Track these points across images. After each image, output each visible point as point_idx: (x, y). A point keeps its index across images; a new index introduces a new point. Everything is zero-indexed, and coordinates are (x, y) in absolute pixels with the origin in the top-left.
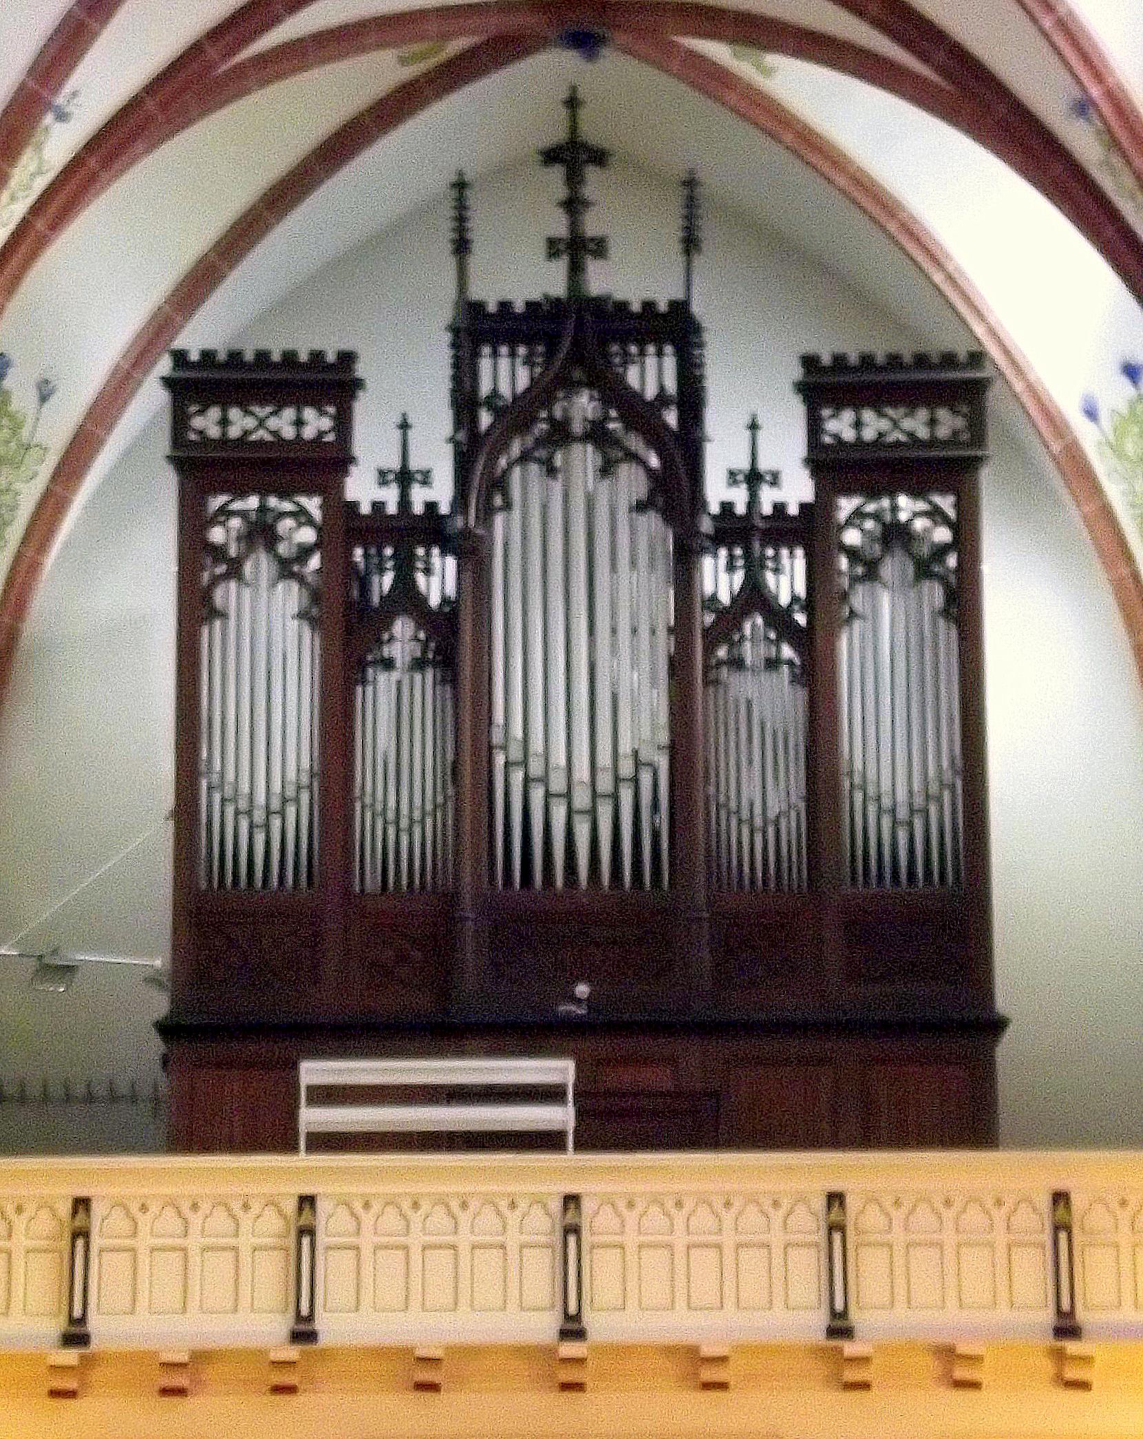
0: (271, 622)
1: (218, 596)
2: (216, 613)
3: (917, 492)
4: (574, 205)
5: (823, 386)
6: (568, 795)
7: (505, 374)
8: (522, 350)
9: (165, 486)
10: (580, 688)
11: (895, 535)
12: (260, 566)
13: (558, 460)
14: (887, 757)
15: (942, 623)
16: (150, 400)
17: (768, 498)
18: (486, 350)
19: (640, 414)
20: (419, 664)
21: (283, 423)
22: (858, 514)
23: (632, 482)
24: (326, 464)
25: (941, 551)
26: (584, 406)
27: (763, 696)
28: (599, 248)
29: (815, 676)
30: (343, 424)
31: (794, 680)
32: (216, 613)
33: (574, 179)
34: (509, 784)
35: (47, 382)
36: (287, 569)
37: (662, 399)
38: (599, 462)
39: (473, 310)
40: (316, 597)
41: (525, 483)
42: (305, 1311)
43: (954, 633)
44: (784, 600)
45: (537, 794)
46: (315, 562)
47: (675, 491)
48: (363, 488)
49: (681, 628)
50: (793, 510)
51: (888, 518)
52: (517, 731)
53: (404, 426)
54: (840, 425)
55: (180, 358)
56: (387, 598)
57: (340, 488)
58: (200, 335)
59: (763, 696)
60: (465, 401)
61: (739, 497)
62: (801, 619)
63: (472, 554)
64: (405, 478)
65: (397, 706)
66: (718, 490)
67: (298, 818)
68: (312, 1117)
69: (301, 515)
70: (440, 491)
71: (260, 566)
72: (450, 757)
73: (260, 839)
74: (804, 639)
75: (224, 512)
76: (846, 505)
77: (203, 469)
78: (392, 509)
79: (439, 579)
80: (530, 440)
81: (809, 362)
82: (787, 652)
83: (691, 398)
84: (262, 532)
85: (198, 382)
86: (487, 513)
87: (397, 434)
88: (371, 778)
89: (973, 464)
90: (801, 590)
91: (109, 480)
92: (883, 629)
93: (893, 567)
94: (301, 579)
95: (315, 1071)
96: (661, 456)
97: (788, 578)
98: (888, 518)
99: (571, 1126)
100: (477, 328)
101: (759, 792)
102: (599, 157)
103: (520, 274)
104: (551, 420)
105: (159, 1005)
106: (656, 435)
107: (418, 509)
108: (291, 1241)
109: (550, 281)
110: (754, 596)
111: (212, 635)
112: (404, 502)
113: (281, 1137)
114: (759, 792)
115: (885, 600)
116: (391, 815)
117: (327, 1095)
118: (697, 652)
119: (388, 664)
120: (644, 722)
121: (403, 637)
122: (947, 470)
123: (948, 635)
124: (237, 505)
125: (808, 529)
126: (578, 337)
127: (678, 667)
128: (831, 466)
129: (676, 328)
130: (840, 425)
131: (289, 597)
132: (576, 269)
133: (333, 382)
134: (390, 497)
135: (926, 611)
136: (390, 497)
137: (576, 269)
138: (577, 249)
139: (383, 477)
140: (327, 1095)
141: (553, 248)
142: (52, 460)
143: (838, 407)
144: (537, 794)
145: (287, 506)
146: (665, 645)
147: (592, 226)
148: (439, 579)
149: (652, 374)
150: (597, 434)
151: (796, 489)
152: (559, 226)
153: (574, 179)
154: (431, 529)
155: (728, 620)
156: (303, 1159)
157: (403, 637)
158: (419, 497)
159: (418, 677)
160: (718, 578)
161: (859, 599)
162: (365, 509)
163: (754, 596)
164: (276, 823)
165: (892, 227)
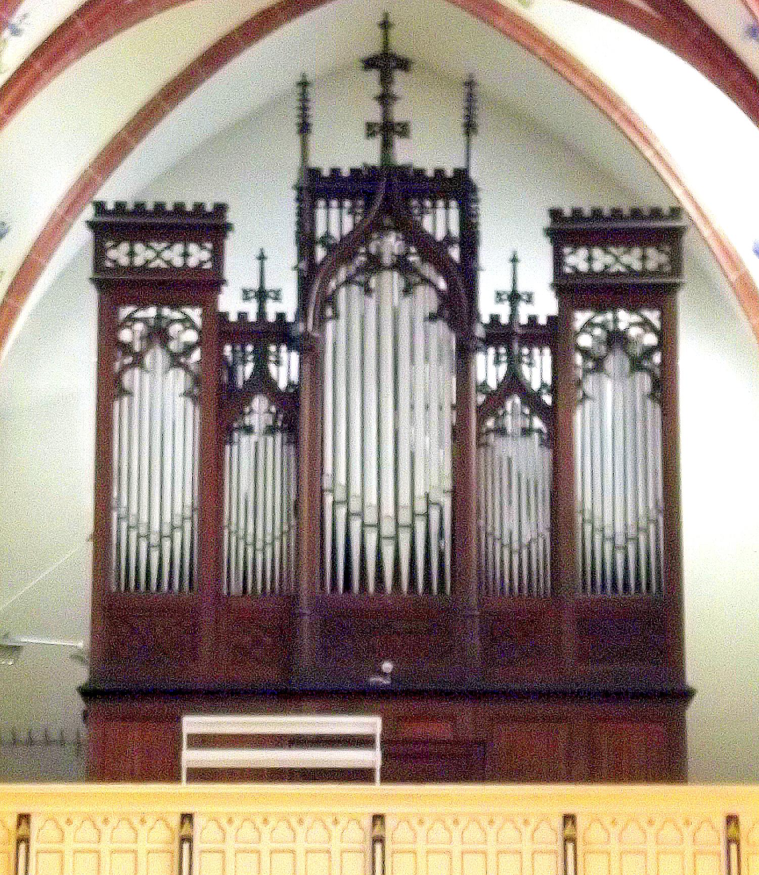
0: (164, 400)
2: (123, 392)
3: (632, 308)
4: (385, 99)
5: (566, 231)
6: (378, 526)
7: (334, 220)
8: (347, 204)
9: (89, 300)
10: (388, 448)
11: (616, 339)
12: (156, 358)
13: (373, 283)
14: (610, 501)
16: (78, 238)
17: (524, 312)
19: (432, 250)
20: (271, 430)
21: (174, 255)
22: (590, 324)
23: (426, 300)
24: (204, 285)
25: (649, 352)
27: (519, 455)
28: (404, 130)
29: (557, 441)
30: (218, 256)
31: (543, 443)
32: (123, 392)
33: (386, 80)
34: (335, 517)
36: (176, 360)
37: (449, 240)
39: (313, 174)
40: (197, 381)
43: (658, 410)
47: (457, 306)
48: (231, 303)
49: (461, 405)
51: (611, 327)
55: (100, 207)
56: (251, 381)
57: (215, 302)
58: (117, 190)
59: (519, 455)
60: (306, 241)
62: (548, 399)
63: (310, 351)
64: (262, 295)
65: (255, 457)
66: (489, 306)
67: (183, 541)
68: (191, 757)
69: (187, 322)
70: (287, 305)
71: (156, 358)
72: (293, 497)
74: (550, 414)
75: (131, 319)
76: (581, 318)
77: (116, 288)
79: (286, 368)
80: (352, 269)
81: (555, 214)
82: (538, 423)
83: (469, 239)
84: (158, 334)
85: (113, 225)
86: (321, 321)
87: (257, 263)
88: (236, 513)
89: (671, 289)
92: (607, 408)
93: (615, 362)
94: (186, 368)
95: (193, 724)
96: (447, 281)
97: (538, 369)
98: (611, 327)
100: (316, 188)
101: (516, 526)
102: (404, 65)
103: (346, 148)
104: (368, 254)
105: (81, 675)
106: (443, 266)
107: (271, 318)
109: (367, 154)
110: (513, 383)
111: (120, 407)
113: (169, 771)
114: (516, 526)
117: (202, 741)
118: (472, 423)
120: (434, 474)
121: (259, 411)
122: (654, 293)
123: (654, 412)
124: (141, 314)
125: (553, 335)
126: (388, 194)
127: (459, 433)
128: (572, 290)
129: (458, 188)
130: (577, 260)
131: (178, 381)
132: (387, 145)
133: (210, 226)
137: (387, 145)
138: (388, 130)
140: (202, 741)
141: (371, 130)
143: (576, 246)
145: (177, 315)
146: (449, 418)
147: (399, 114)
148: (286, 368)
149: (441, 221)
150: (401, 265)
151: (545, 306)
152: (375, 114)
153: (386, 80)
154: (281, 332)
155: (495, 401)
157: (259, 411)
158: (272, 310)
159: (270, 439)
160: (488, 369)
161: (589, 385)
162: (233, 318)
163: (513, 383)
164: (167, 544)
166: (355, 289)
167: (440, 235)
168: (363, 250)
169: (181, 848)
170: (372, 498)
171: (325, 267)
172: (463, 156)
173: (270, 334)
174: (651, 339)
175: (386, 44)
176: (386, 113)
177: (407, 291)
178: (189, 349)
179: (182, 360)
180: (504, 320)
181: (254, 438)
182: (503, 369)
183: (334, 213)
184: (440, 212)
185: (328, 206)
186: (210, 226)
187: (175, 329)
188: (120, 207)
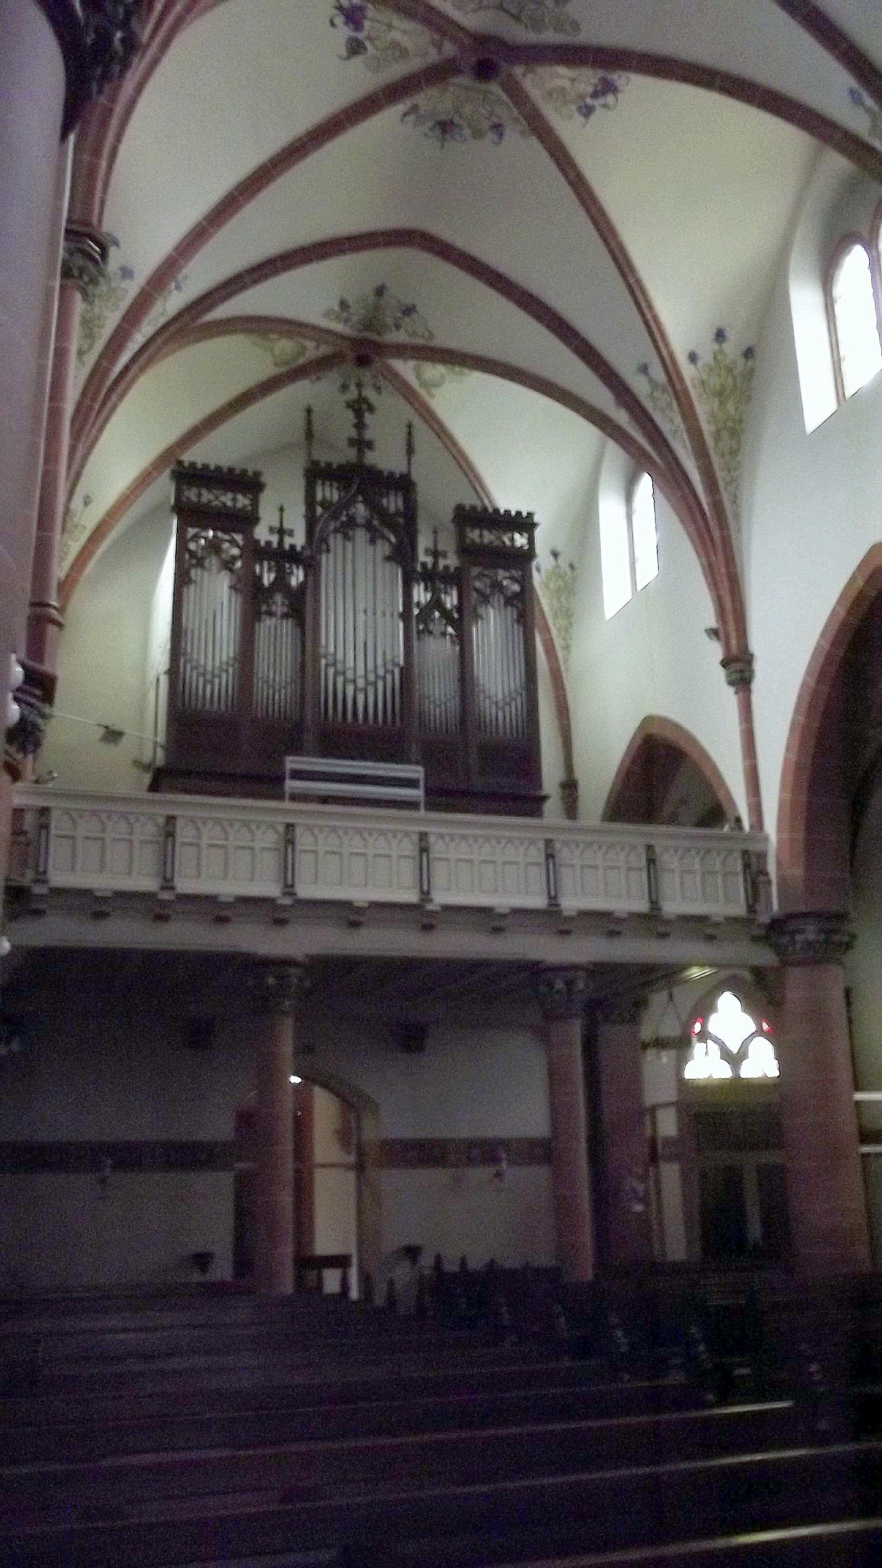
0: (218, 591)
7: (327, 492)
12: (213, 562)
13: (351, 533)
18: (320, 482)
20: (285, 616)
21: (227, 499)
23: (382, 548)
26: (361, 510)
27: (438, 650)
29: (463, 640)
30: (255, 504)
31: (453, 642)
35: (88, 497)
36: (227, 565)
40: (239, 580)
43: (521, 629)
45: (340, 680)
46: (239, 564)
53: (282, 509)
54: (192, 494)
55: (180, 463)
57: (251, 532)
58: (200, 454)
60: (310, 502)
61: (429, 560)
62: (456, 615)
63: (312, 567)
64: (281, 532)
65: (276, 632)
66: (423, 557)
68: (291, 785)
69: (233, 542)
70: (298, 539)
71: (213, 562)
72: (299, 659)
75: (196, 537)
76: (475, 571)
78: (275, 545)
80: (338, 524)
82: (450, 630)
87: (277, 514)
91: (115, 543)
94: (231, 570)
95: (292, 763)
96: (396, 537)
97: (450, 600)
98: (494, 578)
99: (422, 799)
100: (315, 474)
104: (347, 515)
106: (393, 527)
107: (287, 546)
109: (351, 455)
111: (190, 592)
113: (280, 797)
117: (298, 775)
121: (279, 603)
123: (518, 630)
124: (203, 534)
128: (466, 551)
132: (361, 453)
133: (249, 483)
134: (275, 539)
136: (275, 539)
137: (361, 453)
139: (271, 530)
140: (298, 775)
142: (87, 534)
143: (473, 527)
144: (340, 680)
145: (226, 537)
147: (368, 435)
149: (393, 503)
150: (368, 526)
151: (451, 561)
153: (359, 413)
154: (293, 556)
156: (287, 805)
158: (288, 541)
159: (285, 622)
160: (421, 594)
161: (481, 610)
162: (263, 543)
164: (217, 681)
167: (392, 509)
173: (283, 557)
177: (372, 541)
179: (229, 565)
182: (429, 596)
184: (392, 498)
186: (249, 483)
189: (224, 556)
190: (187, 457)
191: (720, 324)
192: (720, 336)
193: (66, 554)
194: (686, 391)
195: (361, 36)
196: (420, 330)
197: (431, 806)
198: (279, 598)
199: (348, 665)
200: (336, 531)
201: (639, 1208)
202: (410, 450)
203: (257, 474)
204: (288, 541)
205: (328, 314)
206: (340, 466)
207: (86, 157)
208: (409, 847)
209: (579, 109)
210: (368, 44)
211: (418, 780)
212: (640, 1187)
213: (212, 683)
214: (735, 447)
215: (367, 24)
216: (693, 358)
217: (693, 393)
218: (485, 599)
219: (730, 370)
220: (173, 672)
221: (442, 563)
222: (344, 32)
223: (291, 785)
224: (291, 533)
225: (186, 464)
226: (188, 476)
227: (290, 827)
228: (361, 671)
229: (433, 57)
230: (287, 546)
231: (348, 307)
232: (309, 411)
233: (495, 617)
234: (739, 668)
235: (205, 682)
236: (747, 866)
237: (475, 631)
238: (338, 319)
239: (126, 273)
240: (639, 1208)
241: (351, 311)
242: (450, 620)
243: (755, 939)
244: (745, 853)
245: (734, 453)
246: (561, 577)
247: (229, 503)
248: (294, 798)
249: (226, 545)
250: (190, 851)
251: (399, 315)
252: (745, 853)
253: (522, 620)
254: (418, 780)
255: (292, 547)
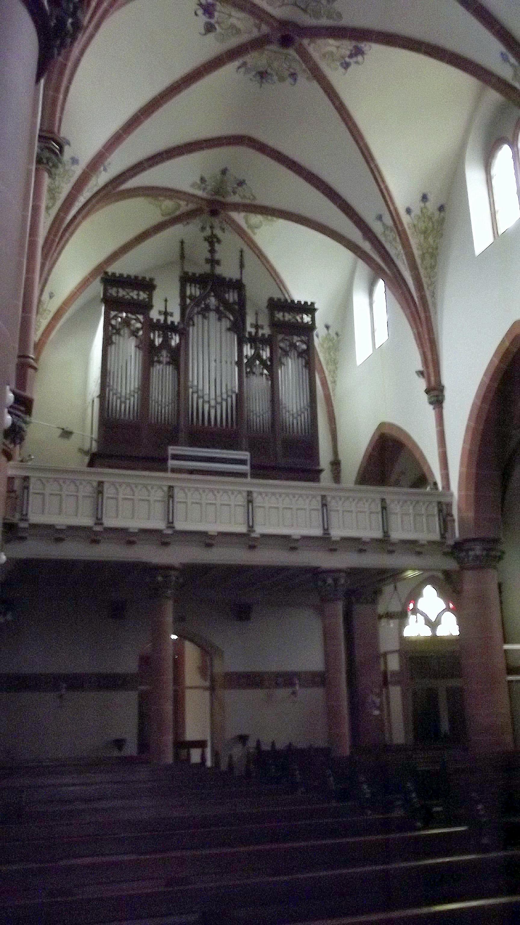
0: (129, 349)
1: (114, 337)
2: (112, 343)
3: (298, 335)
6: (209, 402)
7: (193, 290)
8: (198, 286)
12: (125, 331)
13: (207, 314)
15: (304, 369)
18: (189, 284)
20: (168, 363)
21: (134, 294)
23: (225, 324)
26: (213, 301)
27: (258, 383)
28: (218, 262)
29: (273, 377)
30: (150, 297)
31: (267, 379)
32: (112, 343)
35: (52, 293)
36: (134, 333)
37: (234, 303)
38: (217, 316)
39: (186, 273)
40: (141, 342)
41: (198, 319)
42: (171, 520)
43: (307, 371)
44: (264, 357)
45: (201, 401)
46: (141, 333)
50: (267, 336)
51: (291, 341)
52: (196, 383)
53: (166, 301)
54: (113, 291)
55: (106, 273)
57: (148, 314)
58: (118, 268)
60: (183, 296)
61: (253, 330)
62: (269, 363)
63: (184, 334)
64: (166, 314)
65: (163, 373)
66: (249, 329)
68: (171, 463)
69: (137, 320)
70: (176, 318)
71: (125, 331)
72: (176, 389)
73: (123, 406)
75: (115, 317)
76: (280, 337)
78: (162, 321)
80: (199, 309)
82: (265, 372)
87: (163, 303)
90: (268, 355)
91: (68, 320)
94: (136, 336)
95: (172, 450)
96: (234, 317)
97: (265, 354)
98: (291, 341)
99: (249, 472)
100: (186, 279)
104: (205, 304)
106: (232, 311)
107: (169, 322)
108: (166, 499)
109: (207, 268)
111: (112, 349)
112: (166, 320)
113: (165, 470)
115: (290, 360)
116: (160, 403)
117: (176, 457)
119: (159, 362)
121: (164, 356)
123: (306, 372)
124: (120, 315)
128: (275, 325)
132: (213, 267)
133: (147, 285)
134: (162, 318)
135: (300, 367)
136: (162, 318)
137: (213, 267)
139: (160, 313)
140: (176, 457)
142: (51, 315)
143: (279, 311)
144: (201, 401)
145: (134, 317)
147: (217, 257)
149: (232, 297)
150: (217, 310)
151: (266, 331)
154: (173, 328)
156: (169, 475)
158: (170, 319)
159: (168, 367)
160: (248, 351)
161: (284, 360)
162: (155, 321)
164: (128, 402)
165: (278, 281)
166: (200, 316)
167: (231, 300)
168: (203, 302)
169: (253, 524)
170: (206, 391)
171: (190, 306)
172: (239, 273)
173: (167, 329)
174: (304, 347)
175: (212, 233)
176: (212, 256)
177: (220, 319)
178: (138, 330)
179: (135, 333)
180: (253, 334)
181: (161, 366)
182: (253, 351)
183: (193, 288)
184: (231, 294)
185: (190, 286)
186: (147, 285)
187: (133, 322)
188: (114, 274)
189: (132, 328)
190: (110, 270)
191: (425, 191)
192: (424, 198)
193: (39, 327)
194: (404, 231)
195: (213, 21)
196: (248, 195)
197: (254, 476)
198: (164, 353)
199: (205, 392)
200: (198, 313)
201: (377, 713)
202: (242, 266)
203: (152, 280)
204: (170, 319)
205: (193, 185)
206: (201, 275)
207: (51, 93)
208: (241, 499)
209: (342, 64)
210: (217, 26)
211: (247, 460)
212: (378, 700)
213: (125, 403)
214: (433, 264)
215: (216, 14)
216: (408, 211)
217: (409, 232)
218: (286, 354)
219: (430, 218)
220: (102, 396)
221: (260, 332)
222: (203, 19)
223: (171, 463)
224: (171, 315)
225: (110, 274)
226: (111, 281)
227: (171, 488)
228: (213, 396)
229: (255, 33)
230: (169, 322)
231: (205, 181)
232: (182, 243)
233: (292, 364)
234: (436, 394)
235: (121, 402)
236: (440, 511)
237: (280, 372)
238: (199, 188)
239: (74, 161)
240: (377, 713)
241: (207, 183)
242: (265, 366)
243: (445, 554)
244: (439, 503)
245: (433, 267)
246: (331, 340)
247: (135, 297)
248: (173, 471)
249: (133, 322)
250: (112, 502)
251: (235, 186)
252: (439, 503)
253: (308, 366)
254: (247, 460)
255: (172, 323)
